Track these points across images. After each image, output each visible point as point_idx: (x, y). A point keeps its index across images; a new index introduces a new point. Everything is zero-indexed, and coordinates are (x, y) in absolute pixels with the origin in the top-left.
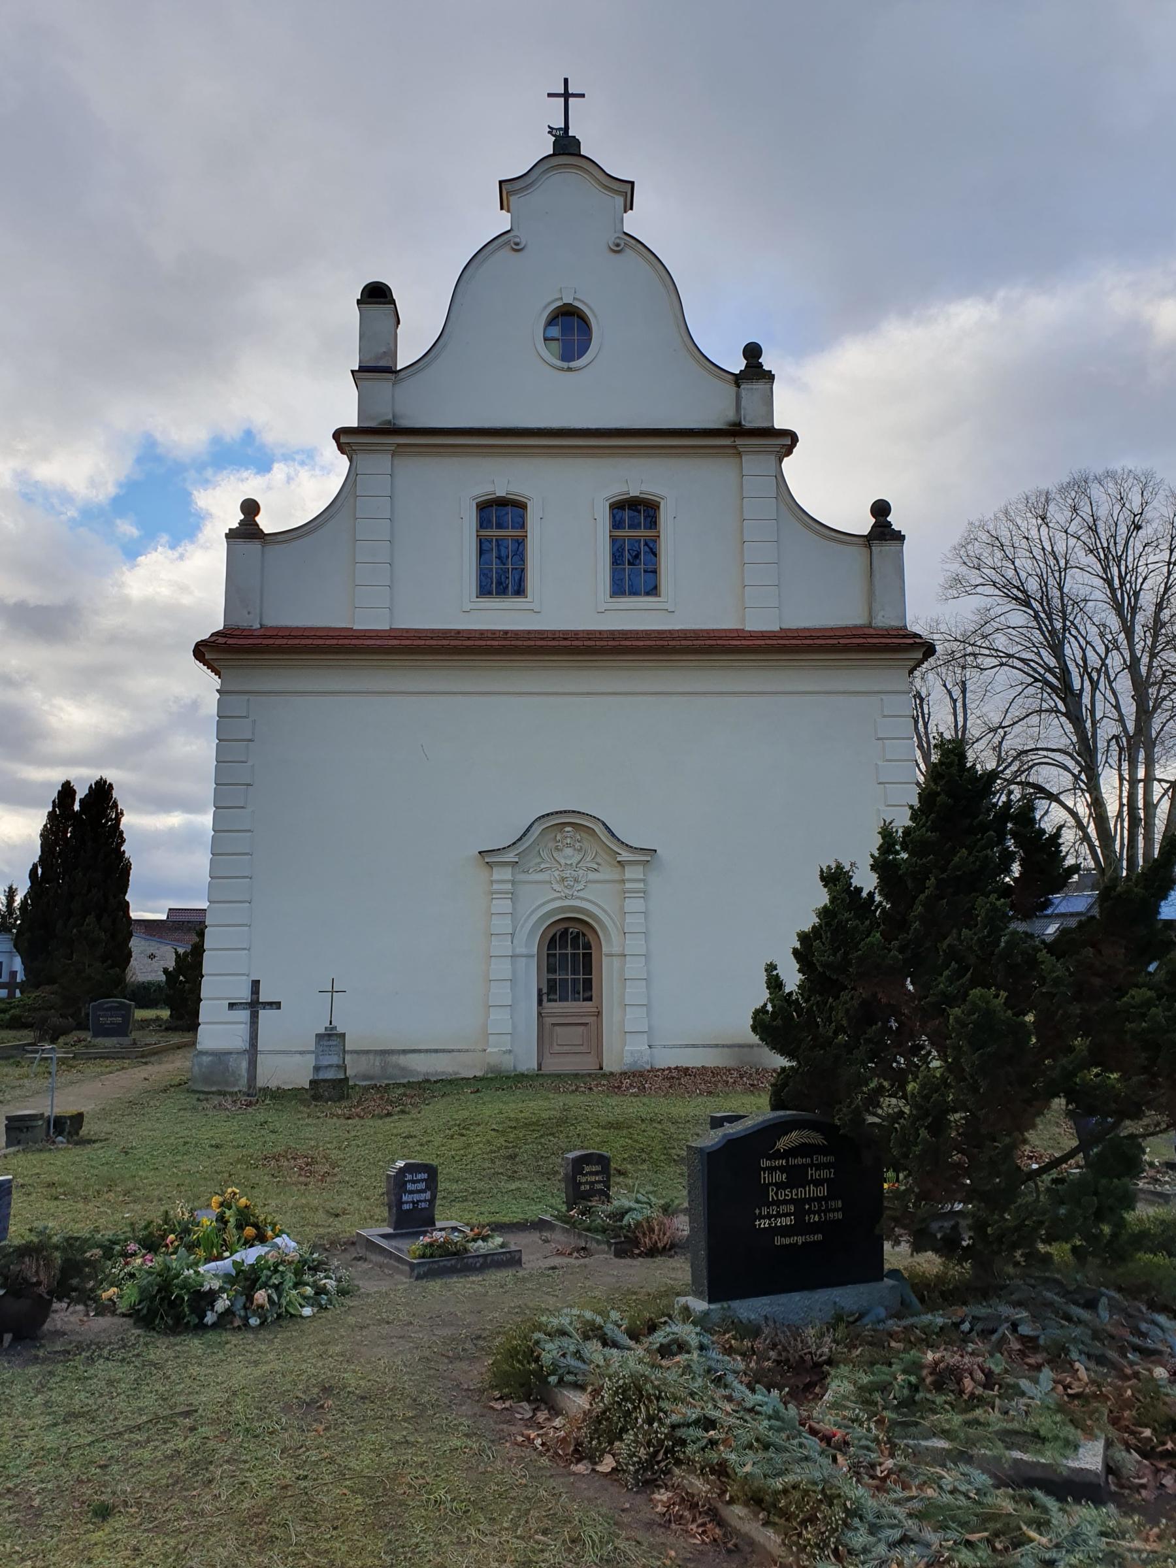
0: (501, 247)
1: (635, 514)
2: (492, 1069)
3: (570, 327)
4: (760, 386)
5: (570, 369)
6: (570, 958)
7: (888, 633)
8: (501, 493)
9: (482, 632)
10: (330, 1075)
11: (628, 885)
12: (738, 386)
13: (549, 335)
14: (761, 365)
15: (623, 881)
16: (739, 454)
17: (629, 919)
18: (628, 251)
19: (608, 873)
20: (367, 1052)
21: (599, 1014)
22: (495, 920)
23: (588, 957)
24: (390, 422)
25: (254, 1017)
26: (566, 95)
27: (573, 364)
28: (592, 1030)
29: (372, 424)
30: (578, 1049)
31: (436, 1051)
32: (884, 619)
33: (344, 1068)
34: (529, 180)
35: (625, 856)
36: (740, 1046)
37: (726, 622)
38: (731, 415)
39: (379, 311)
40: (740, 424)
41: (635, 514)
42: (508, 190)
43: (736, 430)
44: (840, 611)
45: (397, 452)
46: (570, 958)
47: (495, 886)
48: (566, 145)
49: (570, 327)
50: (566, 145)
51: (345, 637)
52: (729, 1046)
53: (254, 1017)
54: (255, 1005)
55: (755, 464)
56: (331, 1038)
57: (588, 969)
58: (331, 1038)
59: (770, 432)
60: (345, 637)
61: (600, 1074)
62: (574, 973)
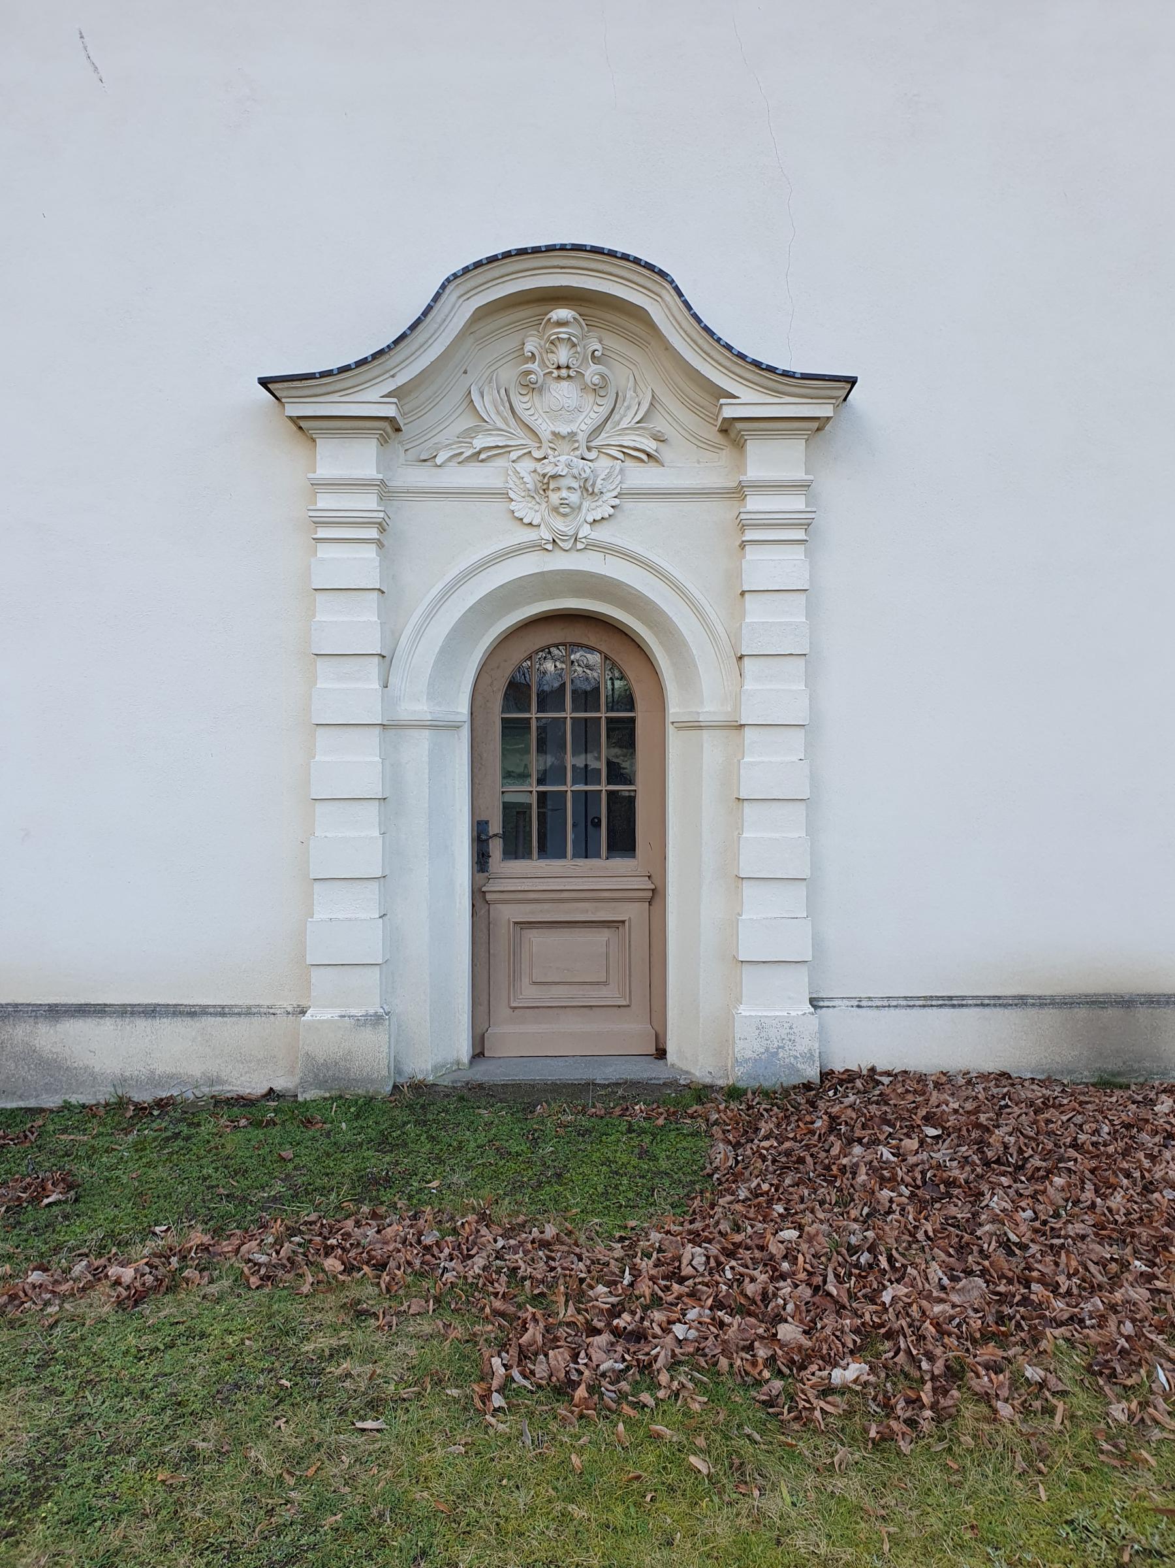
2: (318, 1073)
6: (567, 747)
11: (755, 503)
15: (739, 492)
19: (691, 466)
21: (655, 896)
31: (151, 1011)
35: (750, 400)
46: (567, 747)
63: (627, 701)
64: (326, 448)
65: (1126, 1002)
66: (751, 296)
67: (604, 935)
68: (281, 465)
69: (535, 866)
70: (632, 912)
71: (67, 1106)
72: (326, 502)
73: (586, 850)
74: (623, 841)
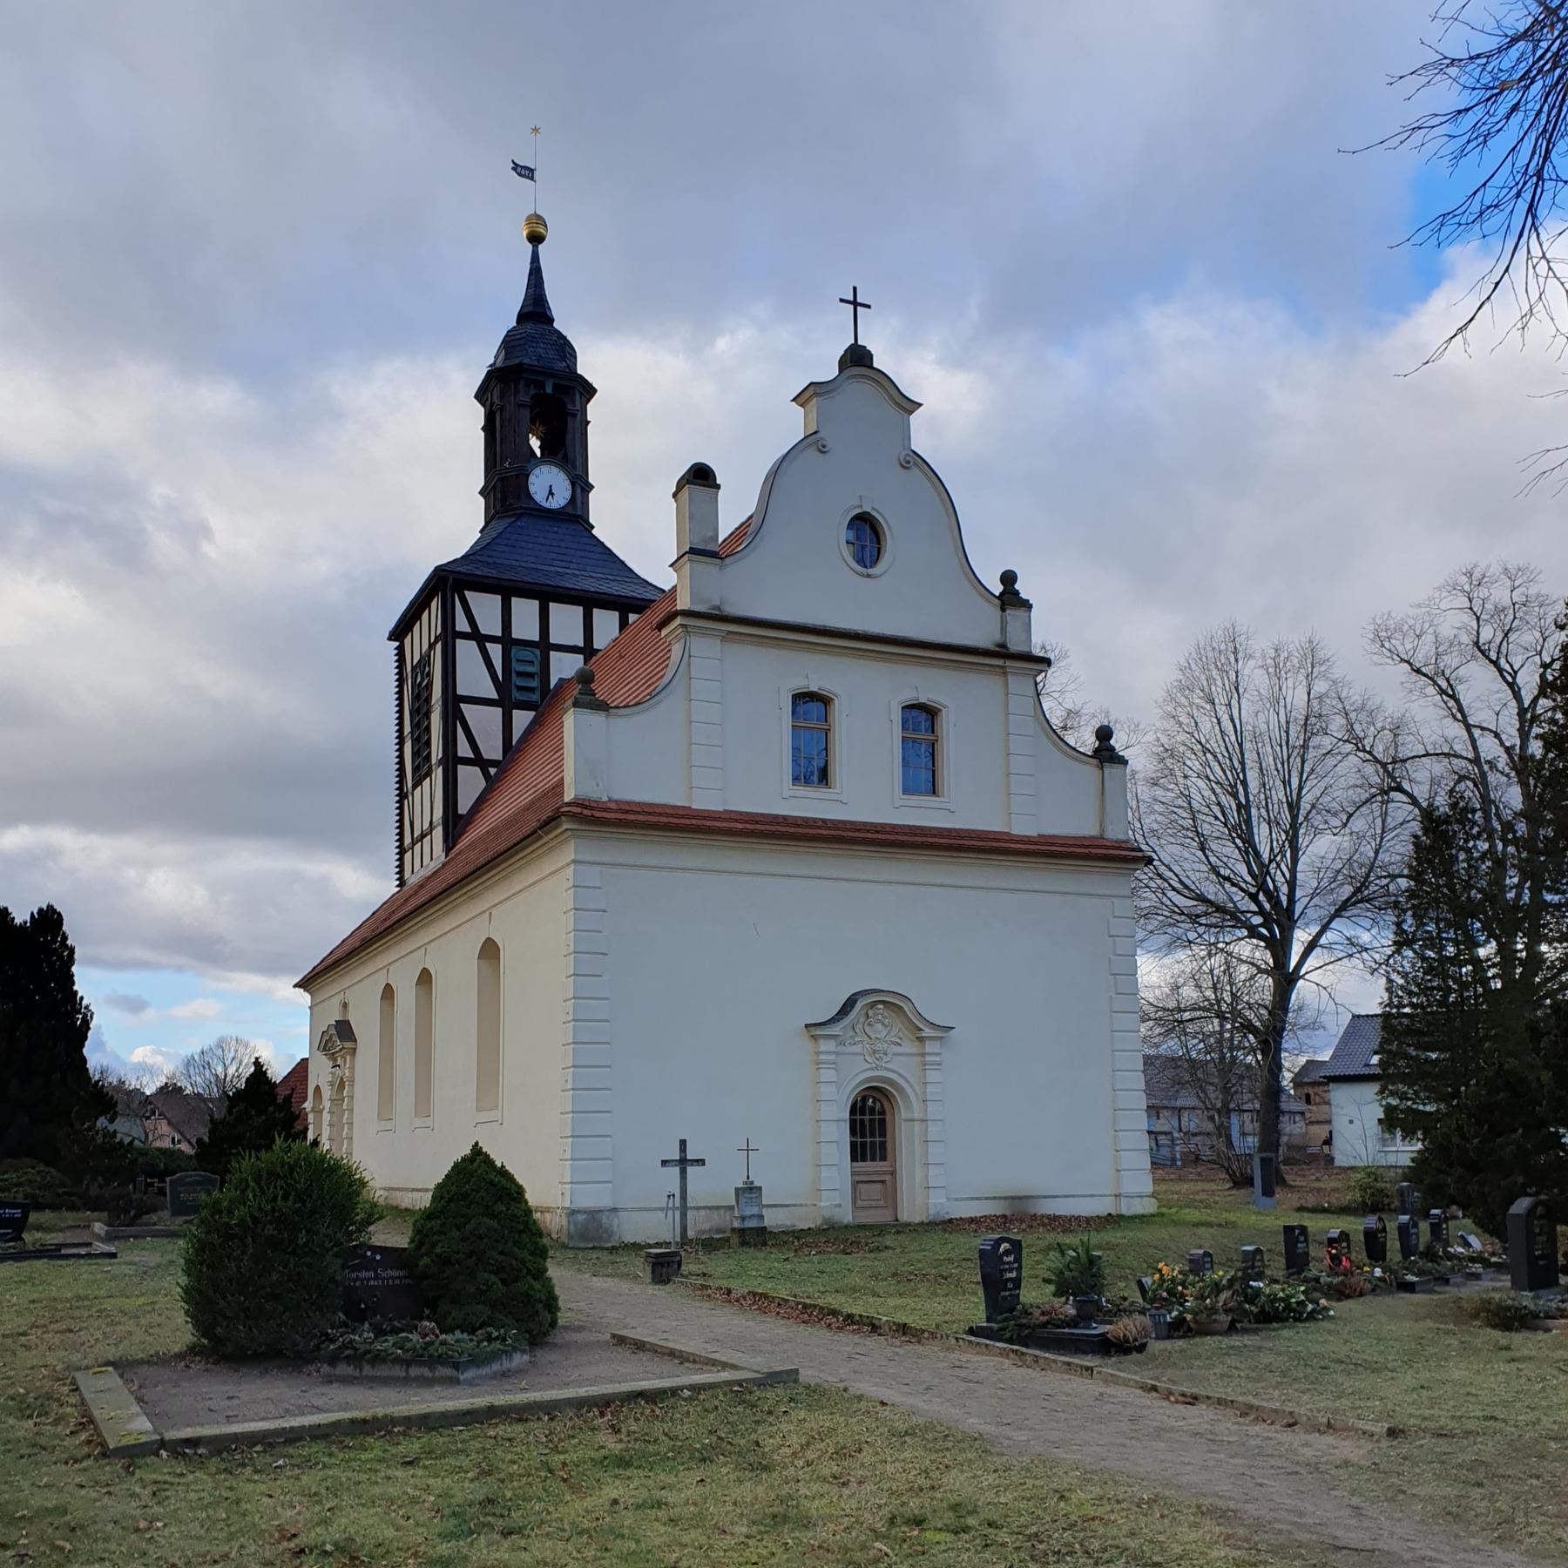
0: (810, 445)
1: (922, 718)
2: (826, 1221)
3: (866, 534)
4: (1021, 613)
5: (869, 576)
6: (871, 1124)
7: (1119, 845)
8: (813, 688)
9: (806, 819)
10: (752, 1224)
11: (928, 1058)
12: (1003, 610)
13: (1326, 1128)
14: (1017, 593)
15: (923, 1055)
16: (1005, 674)
17: (930, 1088)
18: (916, 471)
19: (909, 1047)
20: (718, 1208)
21: (893, 1173)
22: (824, 1088)
23: (883, 1122)
24: (718, 608)
25: (683, 1173)
26: (855, 303)
27: (871, 571)
28: (889, 1186)
29: (697, 608)
30: (874, 1203)
31: (775, 1206)
32: (1114, 833)
33: (761, 1217)
34: (830, 387)
35: (928, 1032)
36: (1013, 1198)
37: (994, 824)
38: (997, 637)
39: (701, 491)
40: (1003, 646)
41: (922, 718)
42: (810, 394)
43: (1001, 652)
44: (1076, 822)
45: (727, 637)
46: (871, 1124)
47: (822, 1057)
48: (857, 358)
49: (866, 534)
50: (857, 358)
51: (682, 817)
52: (1005, 1198)
53: (683, 1173)
54: (683, 1162)
55: (1018, 684)
56: (750, 1191)
57: (883, 1134)
58: (750, 1191)
59: (1029, 658)
60: (682, 817)
61: (901, 1228)
62: (872, 1135)
63: (883, 1112)
64: (822, 1042)
65: (1020, 1198)
66: (930, 1007)
67: (879, 1186)
68: (809, 1045)
69: (868, 1163)
70: (887, 1178)
71: (375, 1418)
72: (822, 1057)
73: (873, 1159)
74: (883, 1158)
